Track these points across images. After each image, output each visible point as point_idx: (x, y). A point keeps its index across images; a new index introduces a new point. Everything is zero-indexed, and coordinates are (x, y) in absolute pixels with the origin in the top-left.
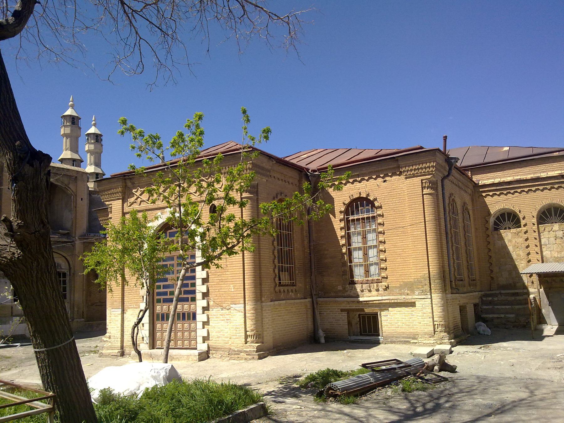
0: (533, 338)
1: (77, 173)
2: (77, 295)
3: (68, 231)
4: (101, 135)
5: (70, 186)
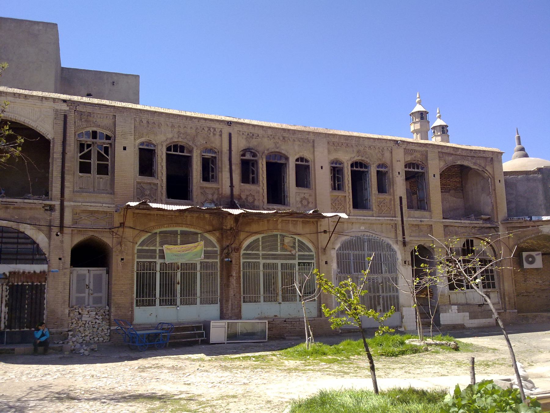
0: (84, 279)
1: (493, 155)
2: (506, 285)
3: (490, 217)
4: (447, 126)
5: (487, 168)
